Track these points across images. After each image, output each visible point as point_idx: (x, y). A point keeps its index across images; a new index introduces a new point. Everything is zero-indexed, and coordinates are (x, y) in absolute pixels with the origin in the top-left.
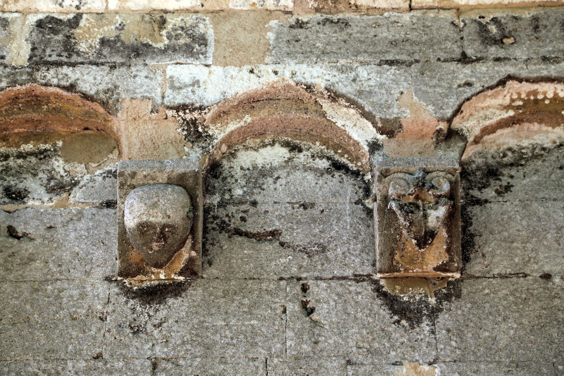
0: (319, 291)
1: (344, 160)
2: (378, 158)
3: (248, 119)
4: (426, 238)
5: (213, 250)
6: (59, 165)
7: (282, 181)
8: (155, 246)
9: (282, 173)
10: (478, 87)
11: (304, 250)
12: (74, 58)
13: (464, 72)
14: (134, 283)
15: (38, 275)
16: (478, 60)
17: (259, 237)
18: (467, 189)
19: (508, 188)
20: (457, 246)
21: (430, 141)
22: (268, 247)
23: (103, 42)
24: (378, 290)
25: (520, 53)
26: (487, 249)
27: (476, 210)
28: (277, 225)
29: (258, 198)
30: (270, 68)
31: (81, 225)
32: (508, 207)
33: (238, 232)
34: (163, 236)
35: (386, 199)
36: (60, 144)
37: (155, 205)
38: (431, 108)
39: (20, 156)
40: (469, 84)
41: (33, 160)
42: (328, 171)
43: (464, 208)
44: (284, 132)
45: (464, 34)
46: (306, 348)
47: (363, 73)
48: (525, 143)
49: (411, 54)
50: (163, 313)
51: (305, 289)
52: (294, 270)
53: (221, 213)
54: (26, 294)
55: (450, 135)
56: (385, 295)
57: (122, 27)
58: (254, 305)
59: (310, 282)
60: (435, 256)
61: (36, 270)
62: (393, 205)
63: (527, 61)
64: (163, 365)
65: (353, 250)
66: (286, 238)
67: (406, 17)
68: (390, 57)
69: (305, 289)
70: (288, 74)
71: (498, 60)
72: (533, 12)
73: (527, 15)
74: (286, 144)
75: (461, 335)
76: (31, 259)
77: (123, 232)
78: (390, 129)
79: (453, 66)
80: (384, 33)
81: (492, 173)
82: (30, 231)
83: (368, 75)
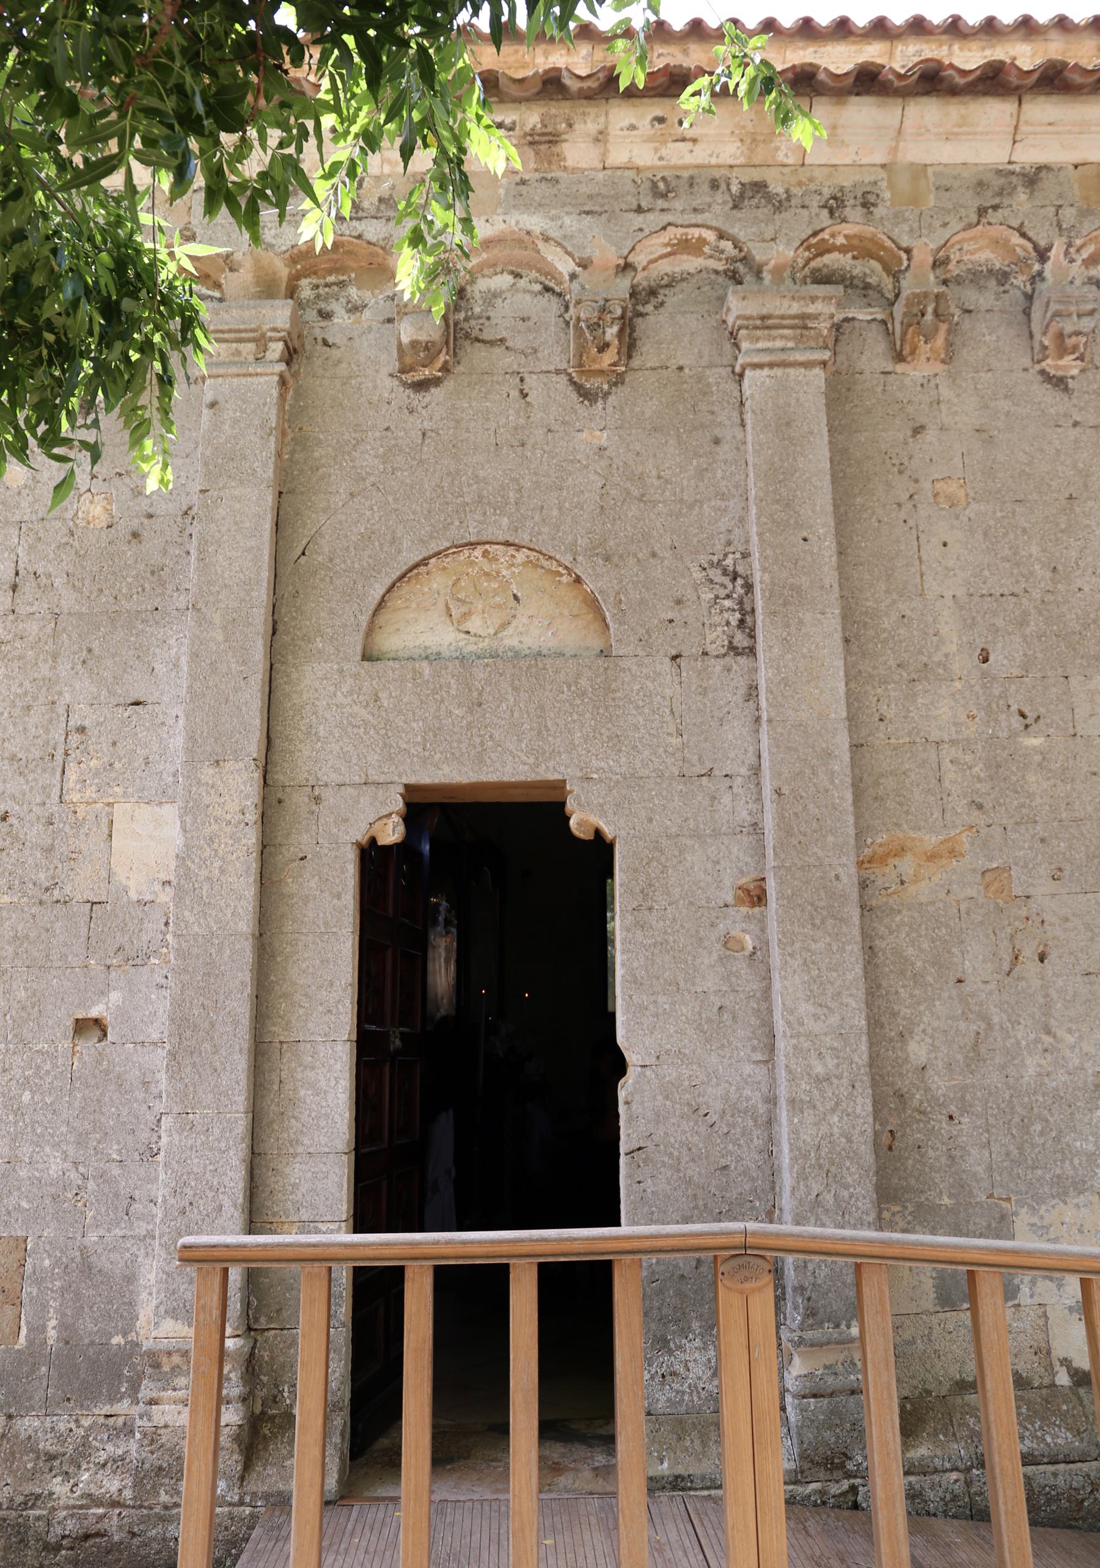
0: (531, 381)
1: (552, 284)
2: (575, 285)
3: (485, 256)
4: (603, 347)
5: (460, 353)
6: (353, 292)
7: (508, 301)
8: (422, 354)
9: (508, 295)
10: (647, 232)
11: (522, 352)
12: (360, 214)
13: (638, 220)
14: (409, 378)
15: (345, 373)
16: (649, 210)
17: (491, 343)
18: (634, 305)
19: (662, 304)
20: (624, 350)
21: (612, 272)
22: (498, 351)
23: (381, 200)
24: (571, 381)
25: (678, 205)
26: (644, 349)
27: (639, 320)
28: (504, 334)
29: (491, 314)
30: (501, 218)
31: (371, 336)
32: (661, 318)
33: (478, 340)
34: (427, 348)
35: (578, 319)
36: (353, 275)
37: (421, 328)
38: (613, 248)
39: (327, 285)
40: (641, 230)
41: (336, 288)
42: (540, 293)
43: (631, 319)
44: (510, 263)
45: (641, 190)
46: (522, 421)
47: (567, 221)
48: (677, 269)
49: (602, 206)
50: (428, 399)
51: (522, 380)
52: (515, 367)
53: (466, 326)
54: (339, 386)
55: (627, 267)
56: (575, 383)
57: (393, 188)
58: (488, 392)
59: (526, 376)
60: (609, 357)
61: (343, 370)
62: (583, 324)
63: (683, 212)
64: (429, 434)
65: (555, 352)
66: (510, 344)
67: (601, 175)
68: (587, 208)
69: (522, 380)
70: (513, 223)
71: (662, 210)
72: (690, 172)
73: (686, 174)
74: (512, 273)
75: (622, 411)
76: (340, 362)
77: (400, 344)
78: (584, 264)
79: (631, 215)
80: (584, 189)
81: (653, 292)
82: (337, 341)
83: (571, 222)
